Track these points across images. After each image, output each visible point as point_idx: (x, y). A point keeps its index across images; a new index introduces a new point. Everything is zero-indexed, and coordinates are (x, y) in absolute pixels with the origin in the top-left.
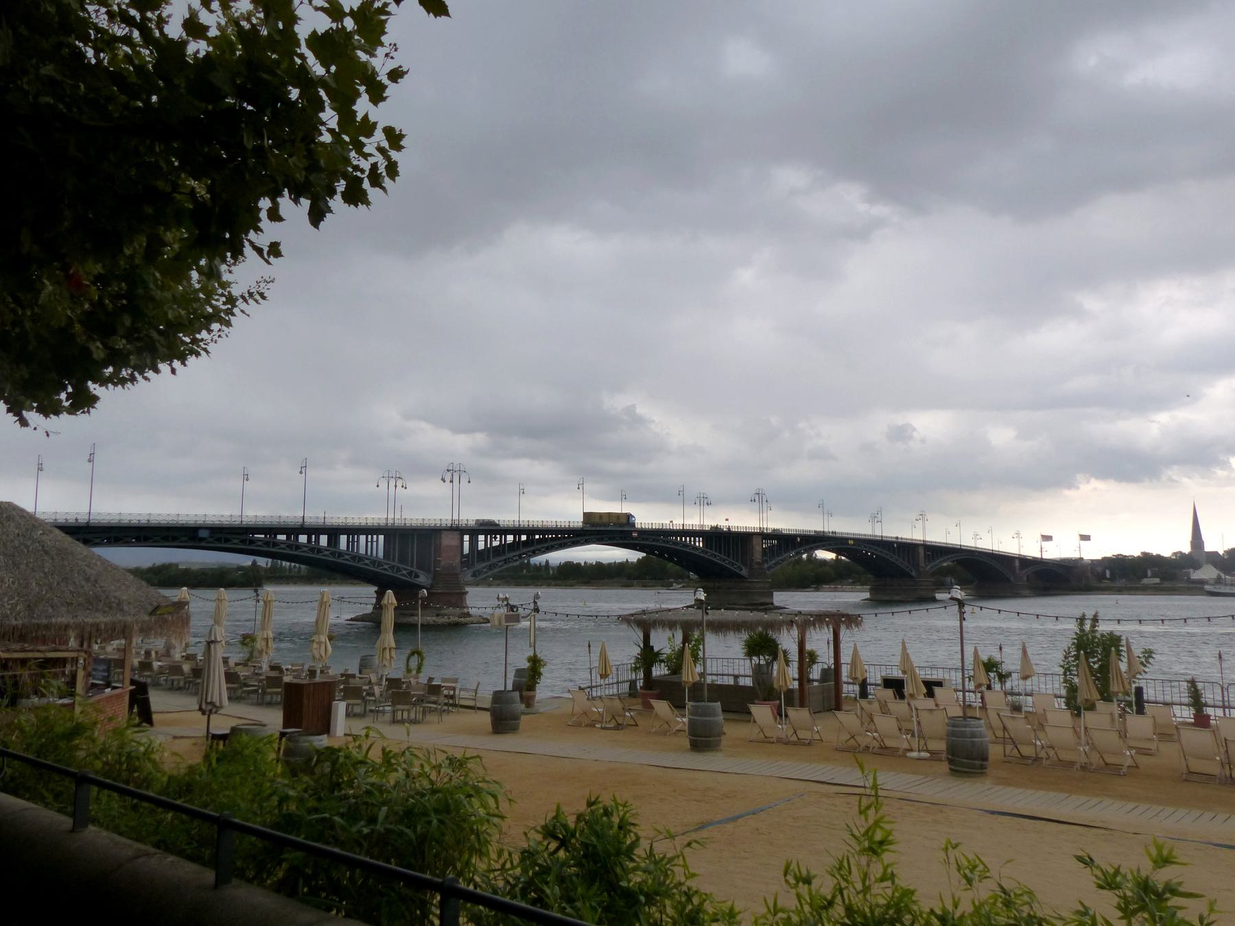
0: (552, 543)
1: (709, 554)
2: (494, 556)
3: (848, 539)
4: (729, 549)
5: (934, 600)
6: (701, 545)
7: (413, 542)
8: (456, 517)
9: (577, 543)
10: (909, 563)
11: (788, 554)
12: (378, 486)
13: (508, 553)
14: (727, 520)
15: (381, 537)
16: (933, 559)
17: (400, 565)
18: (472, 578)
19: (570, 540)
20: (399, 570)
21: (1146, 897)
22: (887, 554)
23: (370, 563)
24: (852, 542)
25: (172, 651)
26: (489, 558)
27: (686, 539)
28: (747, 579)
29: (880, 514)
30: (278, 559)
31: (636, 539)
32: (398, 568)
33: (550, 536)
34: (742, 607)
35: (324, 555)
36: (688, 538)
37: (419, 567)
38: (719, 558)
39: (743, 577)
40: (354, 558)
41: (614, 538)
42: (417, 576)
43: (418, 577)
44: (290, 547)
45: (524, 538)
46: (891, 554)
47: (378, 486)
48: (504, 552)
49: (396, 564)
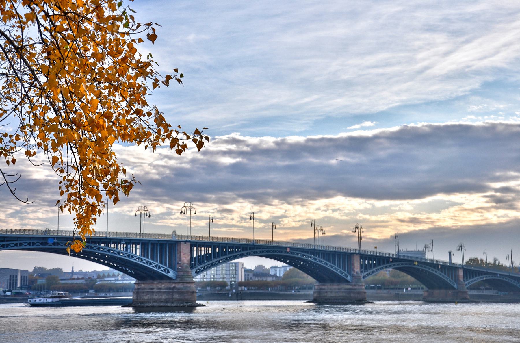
0: (236, 254)
1: (334, 268)
3: (389, 258)
10: (452, 279)
11: (306, 258)
12: (195, 213)
13: (214, 259)
14: (376, 247)
16: (467, 278)
17: (160, 265)
18: (170, 271)
20: (151, 264)
23: (152, 264)
25: (12, 321)
29: (431, 244)
34: (23, 283)
35: (26, 243)
37: (170, 267)
38: (334, 268)
41: (34, 244)
42: (168, 272)
43: (169, 272)
47: (195, 213)
48: (211, 259)
49: (158, 263)
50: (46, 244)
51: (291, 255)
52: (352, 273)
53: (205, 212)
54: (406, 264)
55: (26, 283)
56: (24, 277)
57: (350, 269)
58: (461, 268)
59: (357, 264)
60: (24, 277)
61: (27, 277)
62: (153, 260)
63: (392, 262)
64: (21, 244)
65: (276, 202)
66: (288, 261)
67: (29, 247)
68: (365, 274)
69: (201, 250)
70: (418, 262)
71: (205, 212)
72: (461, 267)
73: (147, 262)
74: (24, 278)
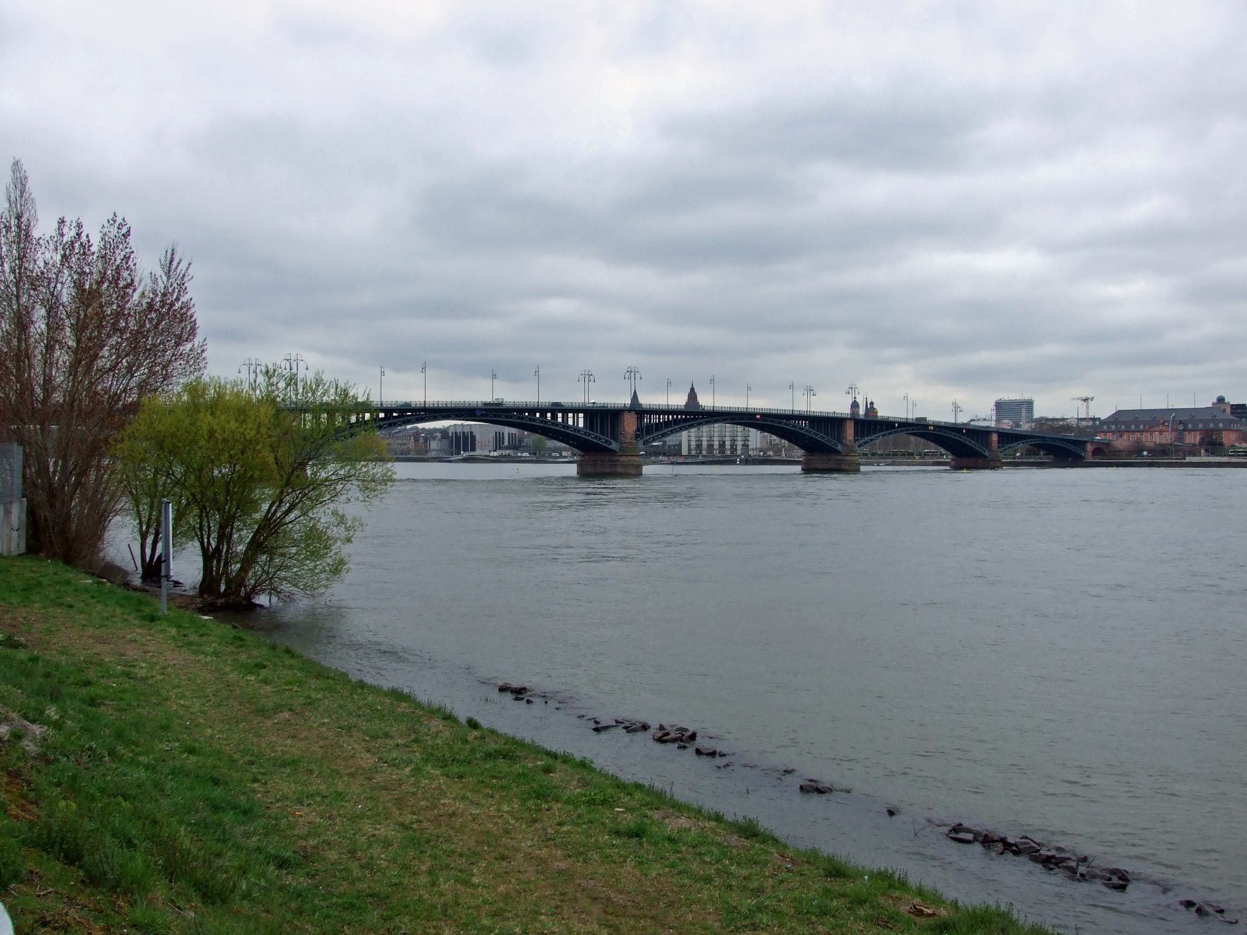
0: (693, 422)
2: (665, 428)
3: (895, 422)
4: (828, 431)
5: (858, 471)
6: (581, 425)
7: (607, 420)
8: (587, 401)
9: (422, 420)
15: (581, 415)
19: (413, 417)
20: (600, 439)
21: (411, 771)
22: (956, 436)
24: (932, 428)
26: (661, 428)
27: (798, 422)
28: (617, 452)
30: (747, 426)
31: (758, 419)
32: (589, 434)
33: (684, 417)
36: (670, 416)
38: (820, 436)
39: (614, 451)
40: (575, 430)
41: (735, 419)
44: (530, 420)
45: (382, 415)
46: (822, 435)
49: (598, 435)
50: (743, 419)
51: (763, 422)
52: (844, 441)
53: (615, 553)
54: (918, 429)
55: (515, 443)
56: (512, 434)
57: (840, 439)
58: (995, 432)
59: (850, 430)
60: (512, 434)
61: (515, 434)
62: (603, 435)
63: (899, 427)
64: (727, 419)
65: (385, 688)
66: (538, 415)
67: (470, 418)
68: (1002, 449)
69: (578, 418)
70: (934, 426)
71: (615, 553)
72: (995, 430)
73: (596, 437)
74: (512, 436)
